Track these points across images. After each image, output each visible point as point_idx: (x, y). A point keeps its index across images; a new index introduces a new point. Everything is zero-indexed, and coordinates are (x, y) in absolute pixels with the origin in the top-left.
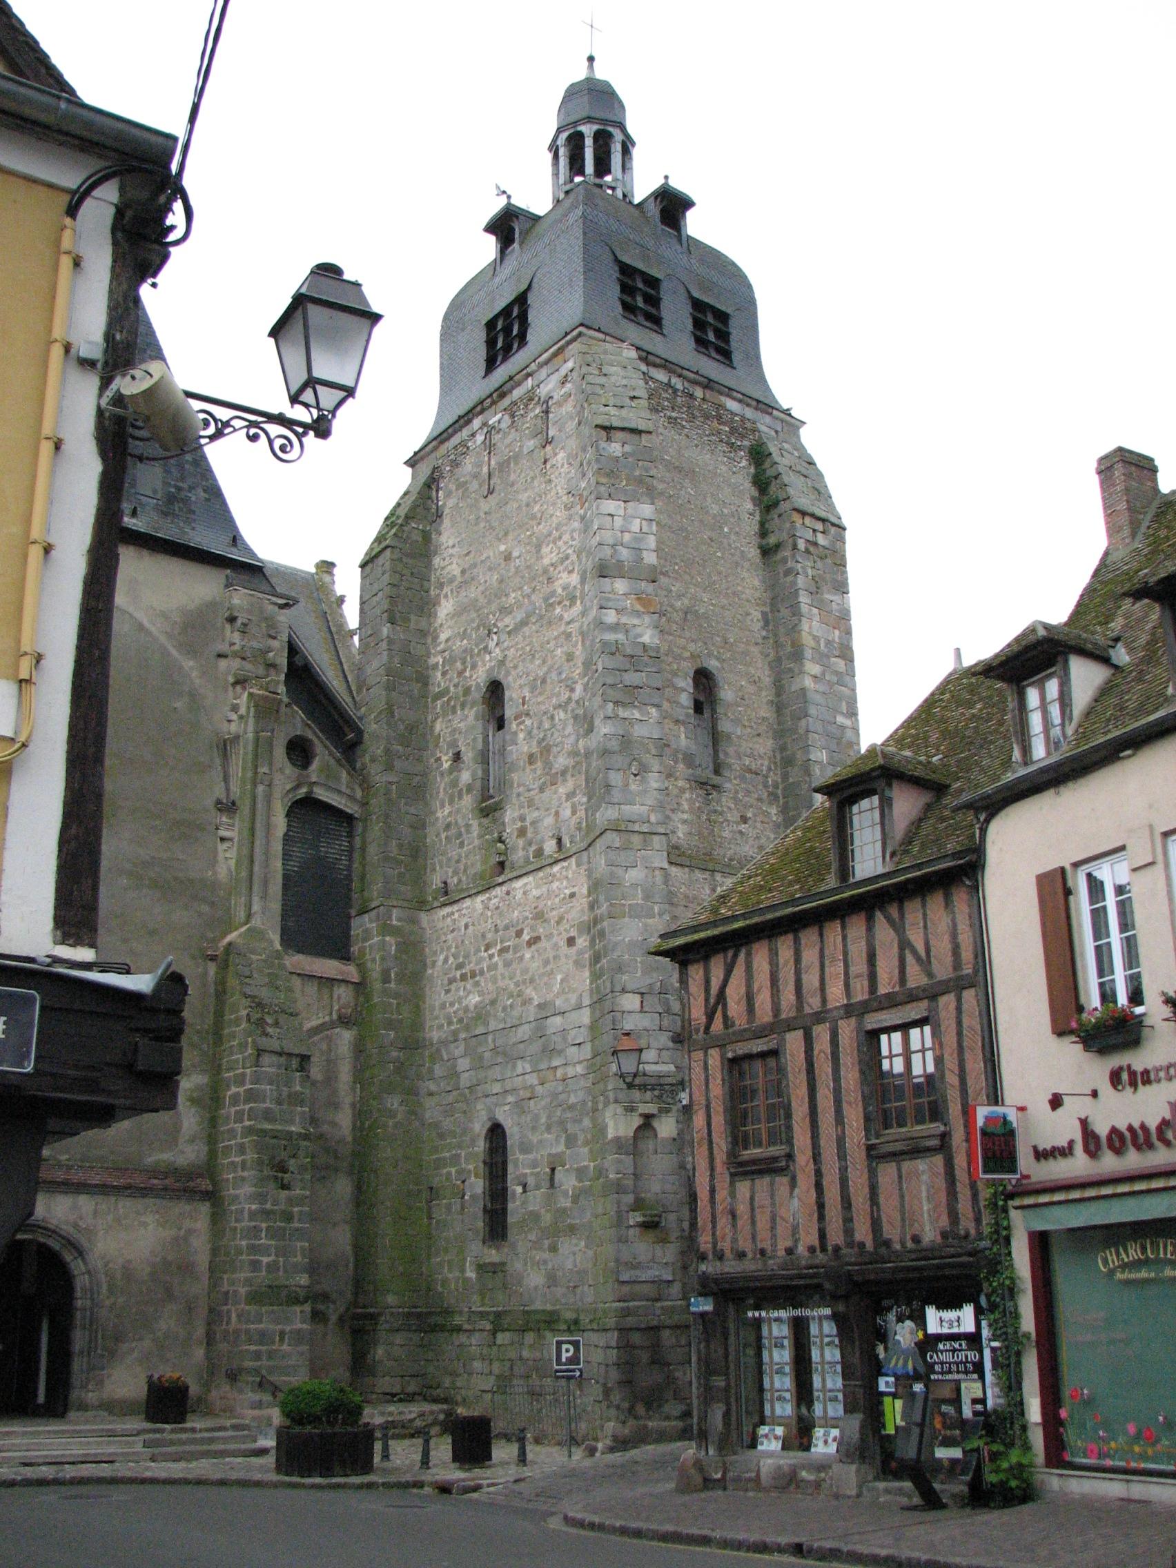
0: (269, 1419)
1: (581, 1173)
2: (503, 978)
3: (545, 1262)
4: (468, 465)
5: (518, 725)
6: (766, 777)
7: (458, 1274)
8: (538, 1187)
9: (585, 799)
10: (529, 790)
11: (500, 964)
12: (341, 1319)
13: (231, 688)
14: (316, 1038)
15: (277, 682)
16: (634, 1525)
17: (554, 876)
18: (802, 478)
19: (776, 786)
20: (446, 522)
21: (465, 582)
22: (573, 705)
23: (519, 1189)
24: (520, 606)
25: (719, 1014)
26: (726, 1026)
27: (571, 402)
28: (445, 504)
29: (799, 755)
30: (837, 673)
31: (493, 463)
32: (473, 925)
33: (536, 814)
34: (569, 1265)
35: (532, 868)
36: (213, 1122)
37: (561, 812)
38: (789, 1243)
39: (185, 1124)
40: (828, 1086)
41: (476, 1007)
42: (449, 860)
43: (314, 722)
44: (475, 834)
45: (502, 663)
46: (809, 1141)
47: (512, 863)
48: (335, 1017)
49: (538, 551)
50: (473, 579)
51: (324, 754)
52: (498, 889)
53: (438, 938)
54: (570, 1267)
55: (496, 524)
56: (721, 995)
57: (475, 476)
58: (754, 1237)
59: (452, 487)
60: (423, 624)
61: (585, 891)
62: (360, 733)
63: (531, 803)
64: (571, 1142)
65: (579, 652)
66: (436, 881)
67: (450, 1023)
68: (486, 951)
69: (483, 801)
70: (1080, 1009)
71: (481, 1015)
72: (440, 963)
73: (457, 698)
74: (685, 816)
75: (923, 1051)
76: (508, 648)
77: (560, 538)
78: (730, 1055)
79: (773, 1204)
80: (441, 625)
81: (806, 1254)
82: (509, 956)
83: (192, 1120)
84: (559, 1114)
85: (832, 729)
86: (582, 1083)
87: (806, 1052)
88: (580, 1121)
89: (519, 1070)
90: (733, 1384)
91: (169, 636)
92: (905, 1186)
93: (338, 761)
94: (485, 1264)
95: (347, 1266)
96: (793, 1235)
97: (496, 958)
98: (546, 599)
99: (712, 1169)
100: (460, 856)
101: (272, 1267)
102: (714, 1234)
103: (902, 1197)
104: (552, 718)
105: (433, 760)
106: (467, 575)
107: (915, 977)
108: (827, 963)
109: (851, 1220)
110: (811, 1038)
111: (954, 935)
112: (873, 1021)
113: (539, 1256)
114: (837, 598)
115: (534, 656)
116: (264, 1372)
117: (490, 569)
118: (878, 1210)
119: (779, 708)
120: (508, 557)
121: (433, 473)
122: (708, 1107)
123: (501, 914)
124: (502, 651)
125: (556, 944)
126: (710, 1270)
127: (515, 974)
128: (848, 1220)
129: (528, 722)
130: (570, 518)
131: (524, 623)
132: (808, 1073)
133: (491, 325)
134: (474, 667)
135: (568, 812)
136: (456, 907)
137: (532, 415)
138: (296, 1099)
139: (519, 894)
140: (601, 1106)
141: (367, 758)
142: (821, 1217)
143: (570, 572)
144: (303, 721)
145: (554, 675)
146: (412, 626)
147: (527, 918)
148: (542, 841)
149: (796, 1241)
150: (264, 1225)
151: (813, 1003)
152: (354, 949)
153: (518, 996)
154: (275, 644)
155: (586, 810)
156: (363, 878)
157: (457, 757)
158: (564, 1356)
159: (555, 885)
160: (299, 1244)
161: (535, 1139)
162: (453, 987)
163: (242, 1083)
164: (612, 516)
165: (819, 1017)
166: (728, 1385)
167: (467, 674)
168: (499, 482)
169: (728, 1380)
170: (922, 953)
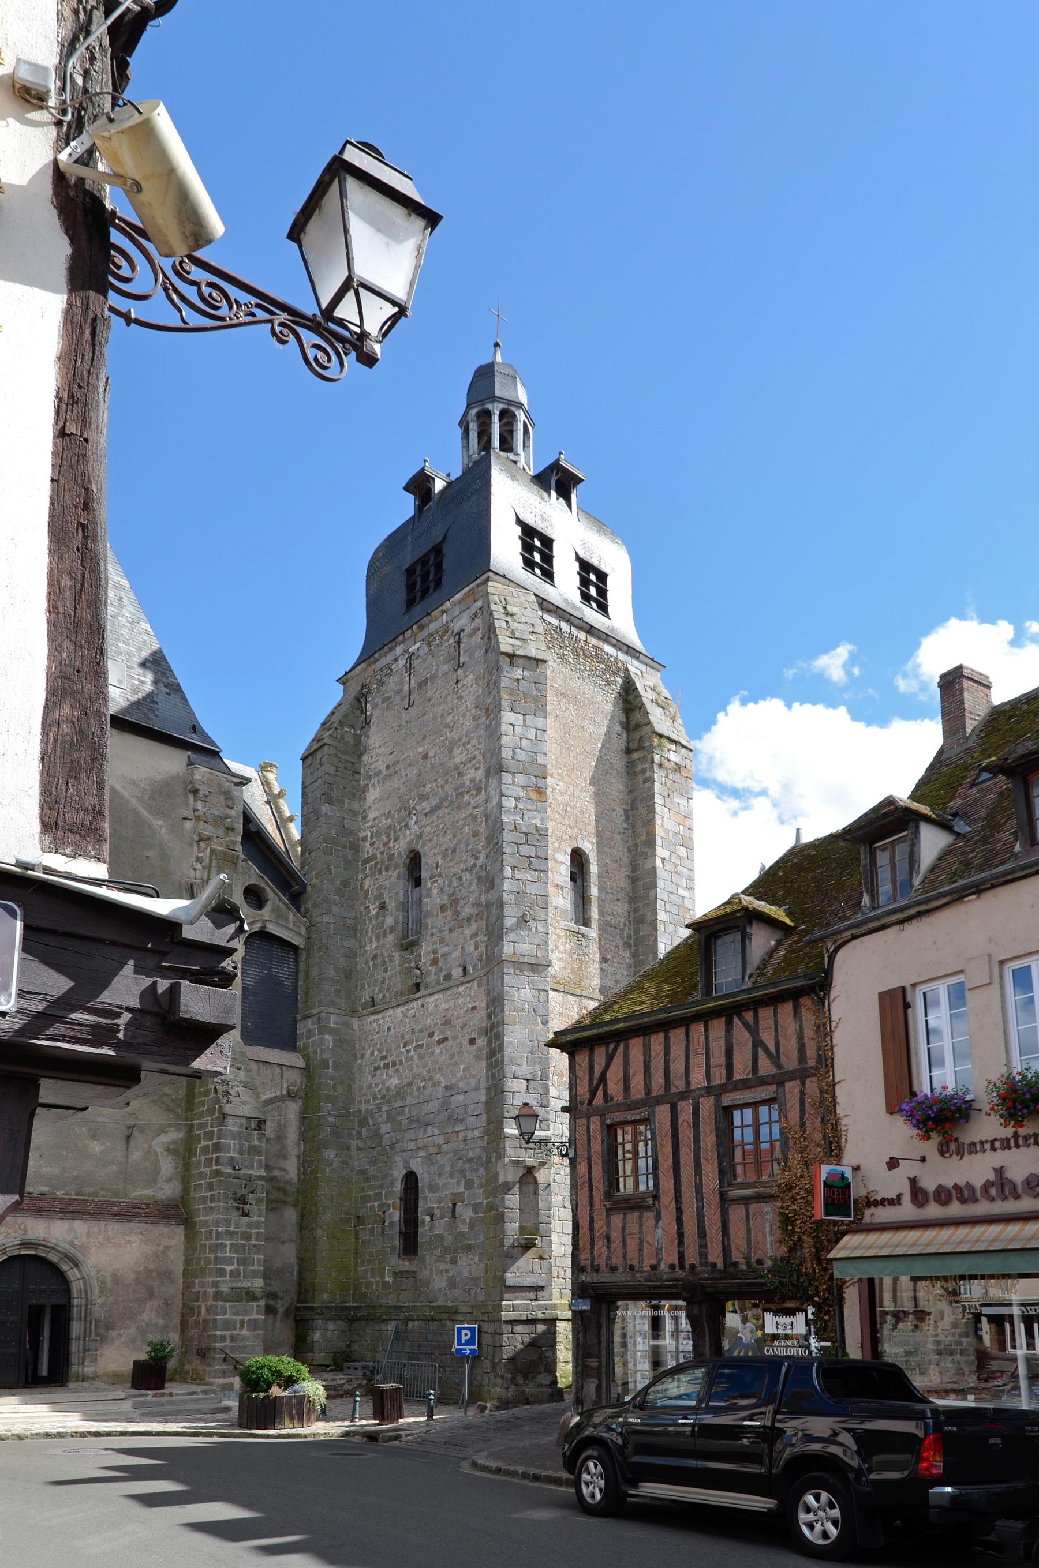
0: (232, 1385)
1: (476, 1207)
2: (418, 1066)
3: (447, 1271)
4: (392, 683)
5: (432, 883)
6: (622, 930)
7: (378, 1279)
8: (442, 1217)
9: (485, 939)
10: (441, 931)
11: (416, 1057)
12: (287, 1313)
13: (195, 844)
14: (271, 1107)
15: (235, 843)
16: (533, 1471)
17: (460, 994)
18: (661, 710)
19: (629, 937)
20: (373, 728)
21: (390, 775)
22: (477, 869)
23: (428, 1218)
24: (436, 794)
25: (600, 1092)
26: (606, 1101)
27: (479, 634)
28: (372, 714)
29: (648, 915)
30: (680, 857)
31: (412, 682)
32: (394, 1028)
33: (446, 949)
34: (465, 1274)
35: (441, 987)
36: (187, 1167)
37: (466, 947)
38: (653, 1262)
39: (163, 1169)
40: (689, 1147)
41: (395, 1087)
42: (376, 981)
43: (265, 874)
44: (397, 963)
45: (419, 836)
46: (672, 1187)
47: (426, 984)
48: (284, 1092)
49: (451, 752)
50: (396, 773)
51: (275, 898)
52: (415, 1003)
53: (367, 1037)
54: (466, 1275)
55: (414, 730)
56: (603, 1078)
57: (398, 692)
58: (624, 1257)
59: (379, 700)
60: (356, 806)
61: (484, 1005)
62: (304, 886)
63: (442, 941)
64: (469, 1184)
65: (482, 829)
66: (366, 997)
67: (375, 1098)
68: (405, 1046)
69: (403, 939)
70: (913, 1094)
71: (400, 1093)
72: (367, 1055)
73: (383, 863)
74: (561, 955)
75: (743, 1126)
76: (425, 826)
77: (469, 743)
78: (608, 1122)
79: (641, 1232)
80: (370, 807)
81: (667, 1270)
82: (423, 1051)
83: (169, 1165)
84: (460, 1164)
85: (673, 898)
86: (479, 1142)
87: (672, 1121)
88: (476, 1170)
89: (429, 1133)
90: (604, 1364)
91: (140, 800)
92: (751, 1222)
93: (286, 905)
94: (401, 1272)
95: (292, 1272)
96: (657, 1256)
97: (412, 1053)
98: (456, 790)
99: (592, 1205)
100: (384, 978)
101: (235, 1274)
102: (592, 1253)
103: (749, 1231)
104: (460, 878)
105: (363, 908)
106: (391, 770)
107: (766, 1067)
108: (691, 1056)
109: (706, 1246)
110: (677, 1110)
111: (801, 1037)
112: (727, 1100)
113: (442, 1266)
114: (683, 801)
115: (445, 832)
116: (227, 1351)
117: (410, 765)
118: (729, 1239)
119: (634, 880)
120: (425, 757)
121: (362, 689)
122: (589, 1159)
123: (417, 1021)
124: (420, 828)
125: (460, 1044)
126: (589, 1279)
127: (427, 1064)
128: (703, 1246)
129: (441, 881)
130: (477, 727)
131: (438, 807)
132: (673, 1136)
133: (410, 572)
134: (396, 839)
135: (472, 948)
136: (380, 1016)
137: (446, 644)
138: (255, 1150)
139: (431, 1007)
140: (493, 1160)
141: (309, 905)
142: (681, 1243)
143: (477, 769)
144: (257, 874)
145: (462, 846)
146: (346, 806)
147: (437, 1024)
148: (451, 968)
149: (660, 1261)
150: (228, 1243)
151: (678, 1085)
152: (300, 1044)
153: (429, 1080)
154: (233, 813)
155: (486, 947)
156: (307, 993)
157: (383, 907)
158: (464, 1339)
159: (461, 1000)
160: (256, 1257)
161: (441, 1182)
162: (378, 1072)
163: (211, 1138)
164: (513, 725)
165: (683, 1096)
166: (600, 1366)
167: (391, 845)
168: (418, 697)
169: (600, 1362)
170: (773, 1050)
